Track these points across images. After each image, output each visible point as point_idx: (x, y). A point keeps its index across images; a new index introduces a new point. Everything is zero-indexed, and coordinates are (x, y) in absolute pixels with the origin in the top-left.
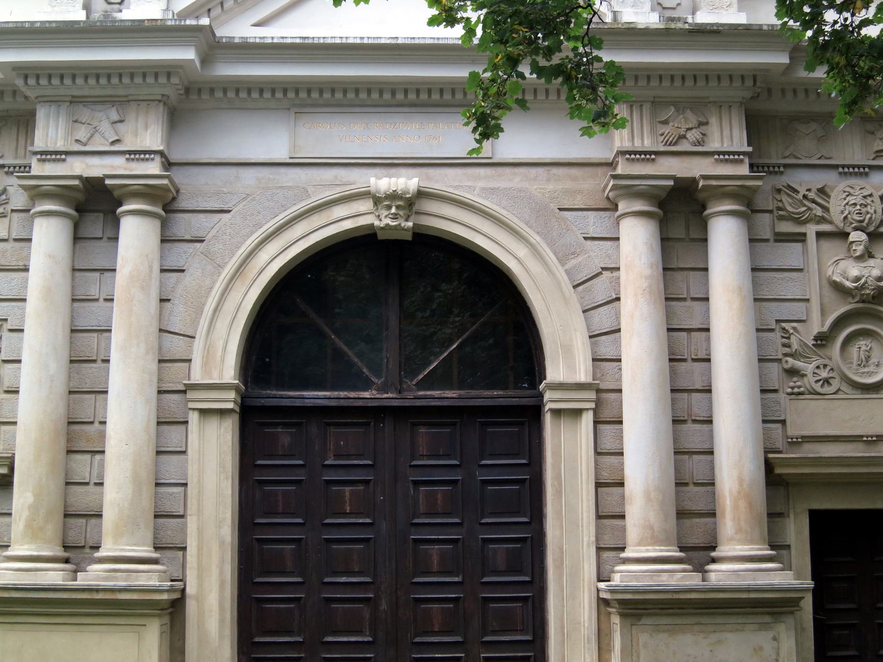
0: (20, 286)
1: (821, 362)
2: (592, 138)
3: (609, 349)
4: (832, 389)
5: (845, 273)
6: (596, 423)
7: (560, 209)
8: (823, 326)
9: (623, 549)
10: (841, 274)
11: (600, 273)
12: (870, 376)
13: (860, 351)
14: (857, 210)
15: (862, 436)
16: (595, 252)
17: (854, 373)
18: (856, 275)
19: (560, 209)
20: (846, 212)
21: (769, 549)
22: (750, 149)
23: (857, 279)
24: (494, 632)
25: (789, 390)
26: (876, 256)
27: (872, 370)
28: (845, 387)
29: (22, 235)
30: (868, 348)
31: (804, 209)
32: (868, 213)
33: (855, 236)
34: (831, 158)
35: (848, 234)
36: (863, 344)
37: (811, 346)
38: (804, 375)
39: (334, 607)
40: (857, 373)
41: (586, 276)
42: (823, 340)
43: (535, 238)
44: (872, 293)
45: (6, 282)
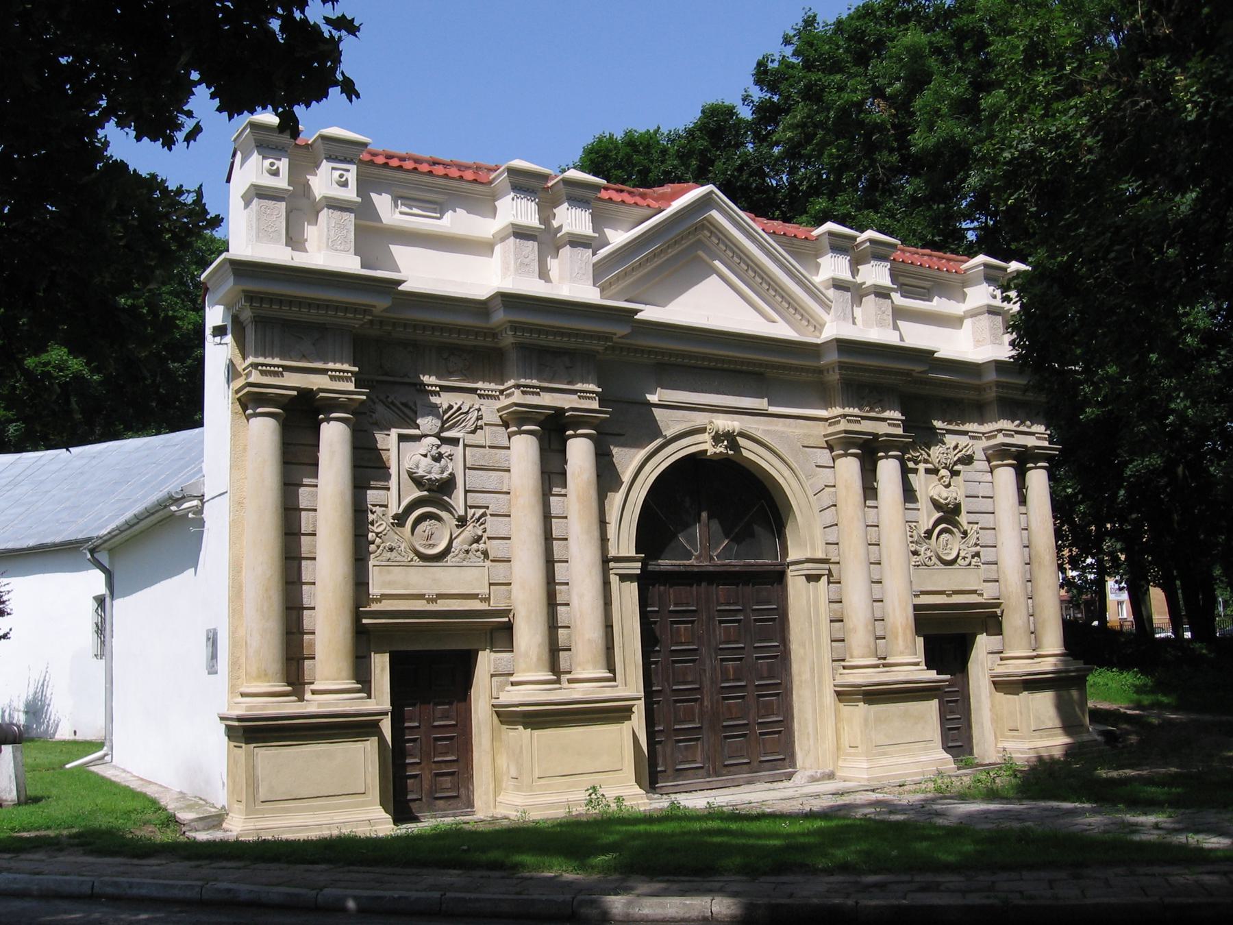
2: (307, 245)
6: (829, 582)
7: (804, 446)
19: (804, 446)
22: (904, 418)
23: (947, 499)
24: (763, 717)
25: (913, 563)
28: (939, 563)
31: (918, 454)
35: (939, 470)
39: (71, 768)
42: (929, 534)
43: (794, 465)
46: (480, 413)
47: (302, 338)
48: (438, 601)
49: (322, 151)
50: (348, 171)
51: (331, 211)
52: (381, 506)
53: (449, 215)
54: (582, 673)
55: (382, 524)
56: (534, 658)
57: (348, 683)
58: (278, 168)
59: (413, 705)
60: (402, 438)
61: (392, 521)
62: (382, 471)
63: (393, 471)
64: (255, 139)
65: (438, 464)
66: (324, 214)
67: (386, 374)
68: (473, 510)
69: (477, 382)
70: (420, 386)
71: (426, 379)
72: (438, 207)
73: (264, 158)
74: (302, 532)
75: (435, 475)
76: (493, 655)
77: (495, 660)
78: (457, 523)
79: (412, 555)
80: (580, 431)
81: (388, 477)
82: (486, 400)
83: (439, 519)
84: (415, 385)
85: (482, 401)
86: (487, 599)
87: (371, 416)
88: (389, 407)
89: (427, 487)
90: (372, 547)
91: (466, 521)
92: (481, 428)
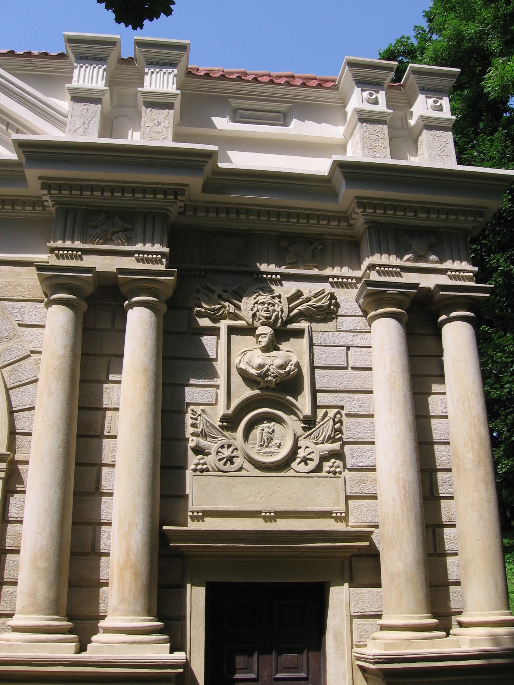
1: (226, 441)
3: (28, 423)
4: (236, 466)
5: (251, 362)
8: (228, 408)
10: (248, 363)
11: (29, 356)
12: (271, 456)
13: (263, 433)
14: (265, 308)
15: (261, 512)
16: (26, 337)
17: (256, 453)
18: (259, 363)
20: (255, 310)
21: (432, 617)
23: (261, 366)
26: (281, 349)
27: (273, 450)
28: (247, 465)
30: (271, 430)
31: (218, 306)
32: (274, 311)
33: (261, 330)
34: (248, 266)
35: (256, 328)
36: (266, 426)
37: (218, 428)
38: (208, 454)
40: (259, 453)
41: (15, 357)
44: (274, 380)
48: (206, 519)
49: (416, 85)
58: (441, 105)
63: (221, 366)
64: (354, 80)
66: (426, 136)
68: (324, 410)
69: (325, 268)
70: (258, 275)
71: (263, 267)
73: (363, 90)
74: (106, 433)
81: (213, 374)
84: (251, 274)
86: (344, 518)
91: (315, 424)
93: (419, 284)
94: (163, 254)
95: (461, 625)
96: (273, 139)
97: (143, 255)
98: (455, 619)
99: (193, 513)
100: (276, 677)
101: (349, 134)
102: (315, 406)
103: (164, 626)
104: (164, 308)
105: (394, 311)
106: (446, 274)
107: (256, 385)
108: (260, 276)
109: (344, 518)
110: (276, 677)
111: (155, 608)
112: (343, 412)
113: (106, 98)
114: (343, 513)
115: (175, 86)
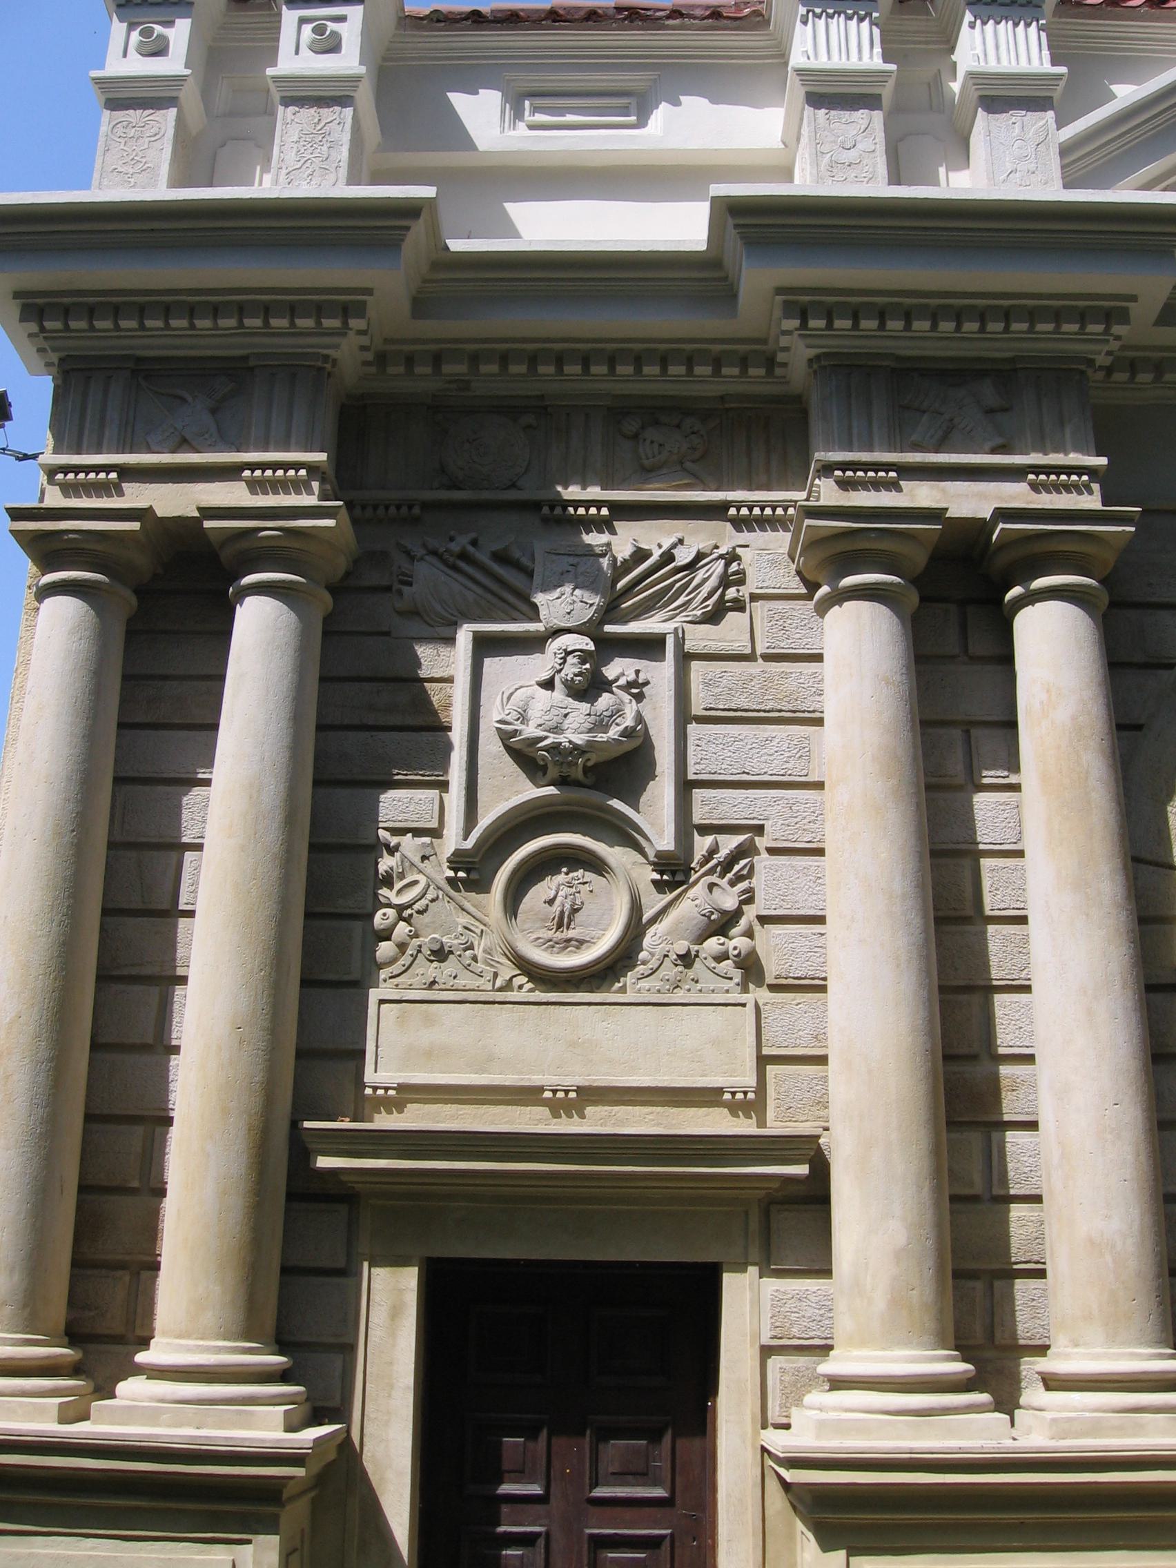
0: (787, 754)
9: (825, 1349)
29: (782, 645)
45: (754, 745)
46: (734, 567)
47: (183, 400)
48: (589, 1110)
50: (342, 19)
51: (292, 109)
52: (417, 832)
53: (661, 115)
54: (1067, 1356)
55: (415, 882)
56: (880, 1301)
57: (219, 1350)
59: (531, 1432)
60: (485, 646)
61: (451, 874)
62: (426, 736)
65: (584, 707)
67: (455, 486)
68: (709, 840)
70: (552, 508)
71: (572, 492)
72: (632, 101)
73: (132, 26)
75: (574, 734)
76: (772, 1285)
77: (778, 1301)
78: (658, 877)
79: (507, 970)
80: (1040, 583)
82: (759, 533)
83: (597, 865)
84: (536, 506)
85: (745, 537)
86: (754, 1105)
87: (400, 593)
88: (455, 568)
89: (553, 772)
90: (385, 949)
91: (688, 870)
92: (738, 606)
93: (947, 509)
94: (312, 468)
95: (1052, 1383)
96: (632, 166)
97: (286, 472)
98: (1031, 1367)
99: (386, 1092)
100: (592, 1494)
101: (792, 139)
102: (686, 827)
103: (974, 1373)
104: (914, 598)
105: (1084, 583)
106: (240, 479)
107: (540, 774)
108: (558, 511)
109: (754, 1105)
110: (592, 1494)
111: (269, 1320)
112: (761, 843)
113: (190, 95)
114: (752, 1092)
115: (878, 49)
